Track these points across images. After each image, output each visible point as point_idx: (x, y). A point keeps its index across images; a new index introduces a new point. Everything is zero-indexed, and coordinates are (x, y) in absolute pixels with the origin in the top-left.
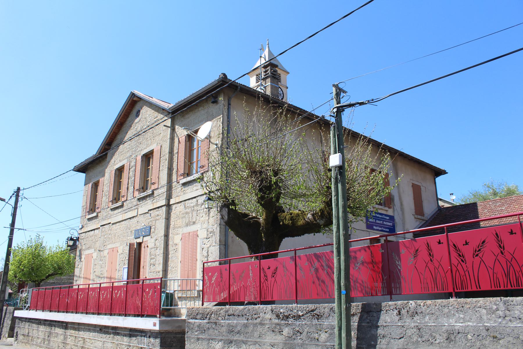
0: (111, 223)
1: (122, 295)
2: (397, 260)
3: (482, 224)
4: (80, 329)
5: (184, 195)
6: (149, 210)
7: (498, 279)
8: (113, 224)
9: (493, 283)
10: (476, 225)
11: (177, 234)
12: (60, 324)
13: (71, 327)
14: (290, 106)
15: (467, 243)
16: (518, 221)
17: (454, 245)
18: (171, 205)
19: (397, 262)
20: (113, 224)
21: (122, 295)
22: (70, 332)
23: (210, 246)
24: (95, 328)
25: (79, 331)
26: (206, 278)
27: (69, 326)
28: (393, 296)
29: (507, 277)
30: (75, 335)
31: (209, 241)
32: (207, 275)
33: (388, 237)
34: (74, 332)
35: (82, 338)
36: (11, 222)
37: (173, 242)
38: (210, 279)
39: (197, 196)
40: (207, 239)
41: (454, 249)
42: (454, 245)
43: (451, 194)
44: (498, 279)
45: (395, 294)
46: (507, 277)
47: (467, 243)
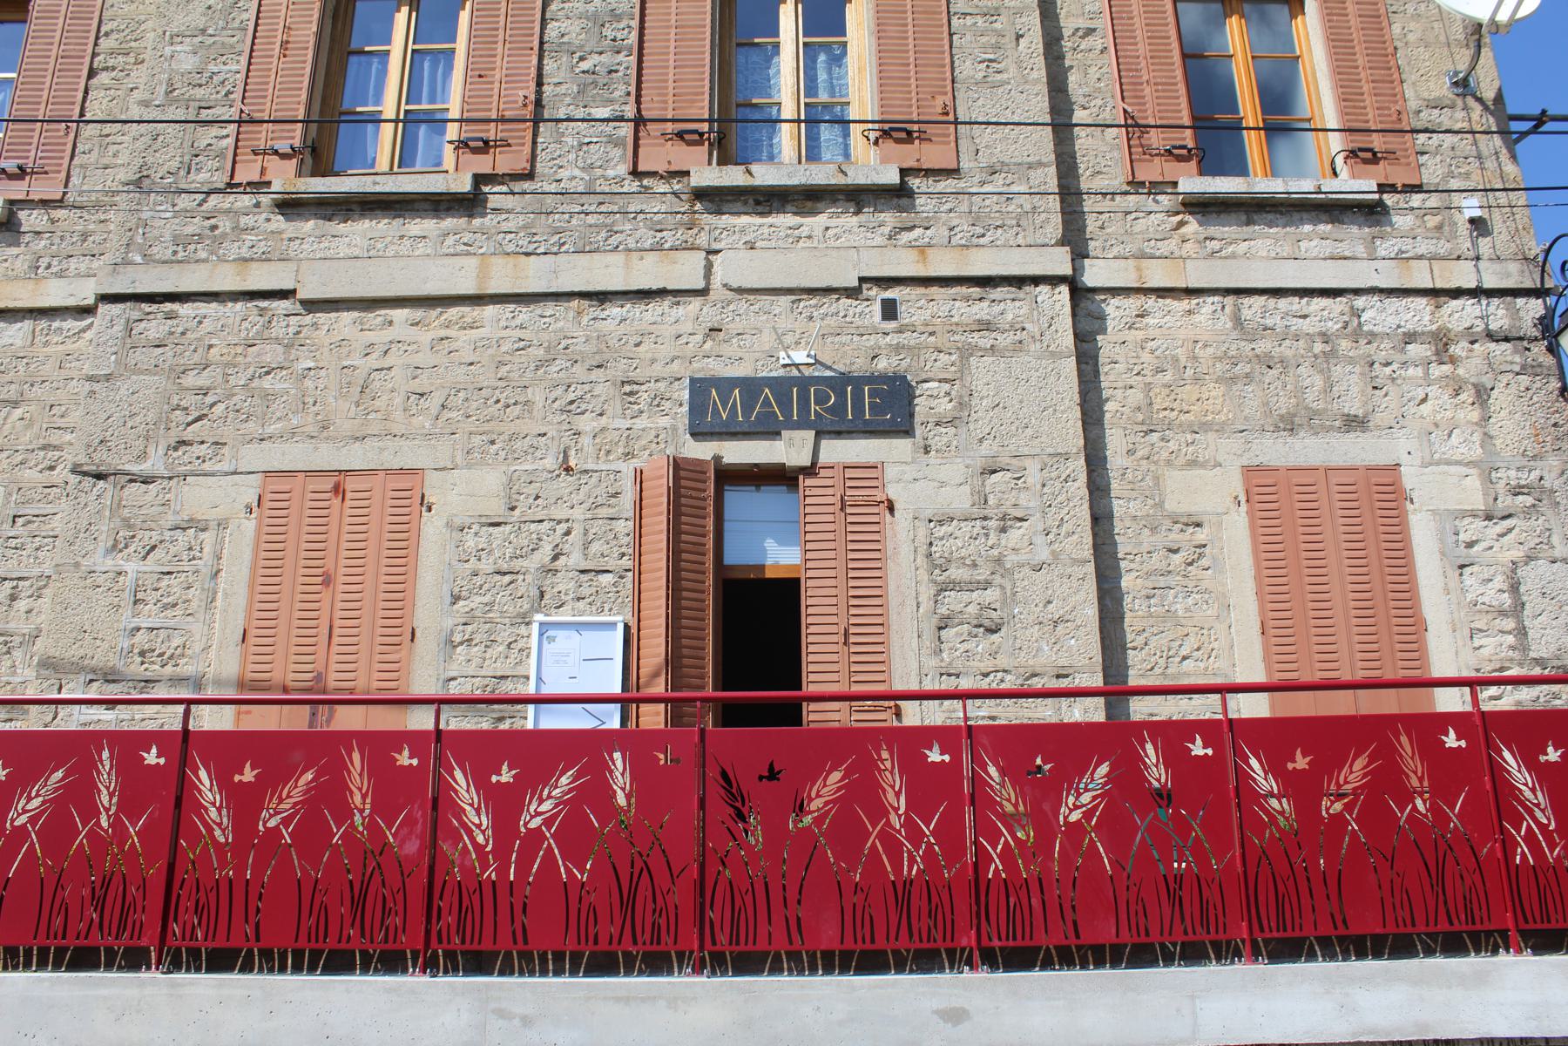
2: (893, 787)
3: (814, 714)
5: (1209, 262)
6: (862, 280)
7: (595, 913)
8: (312, 305)
9: (846, 917)
10: (790, 714)
11: (1193, 463)
15: (773, 775)
17: (724, 775)
18: (1094, 290)
19: (891, 795)
20: (312, 305)
23: (1529, 559)
29: (1173, 905)
31: (1510, 530)
33: (192, 706)
37: (1161, 505)
39: (1357, 292)
40: (1489, 518)
41: (722, 791)
42: (724, 775)
44: (595, 913)
46: (1173, 905)
47: (773, 775)
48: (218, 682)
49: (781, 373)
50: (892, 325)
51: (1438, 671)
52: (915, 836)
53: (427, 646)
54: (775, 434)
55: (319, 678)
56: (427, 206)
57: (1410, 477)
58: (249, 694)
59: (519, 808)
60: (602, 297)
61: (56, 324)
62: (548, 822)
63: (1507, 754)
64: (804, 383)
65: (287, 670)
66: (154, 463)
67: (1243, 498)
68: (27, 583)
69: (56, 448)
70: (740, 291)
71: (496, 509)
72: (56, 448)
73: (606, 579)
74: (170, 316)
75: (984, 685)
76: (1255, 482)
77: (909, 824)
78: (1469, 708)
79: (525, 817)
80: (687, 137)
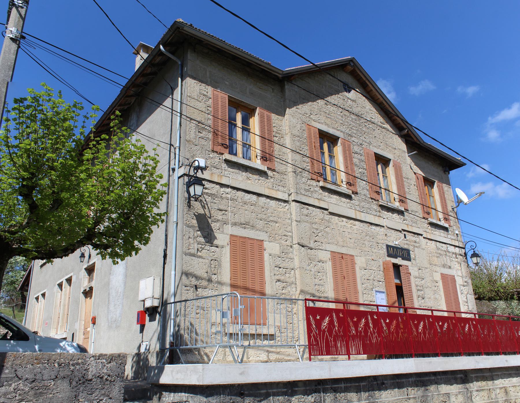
0: (423, 236)
1: (473, 329)
4: (494, 377)
6: (402, 229)
8: (331, 214)
12: (449, 376)
13: (476, 377)
14: (164, 42)
16: (210, 122)
20: (331, 214)
21: (473, 329)
22: (474, 386)
24: (517, 371)
25: (493, 379)
26: (313, 322)
27: (473, 375)
28: (351, 356)
30: (488, 388)
32: (315, 318)
34: (484, 383)
35: (501, 388)
36: (165, 265)
38: (318, 324)
43: (60, 92)
45: (352, 355)
48: (331, 299)
49: (394, 245)
50: (405, 239)
51: (462, 311)
52: (374, 333)
53: (360, 294)
54: (396, 258)
55: (347, 299)
56: (343, 195)
57: (266, 244)
58: (336, 302)
59: (321, 325)
60: (371, 224)
61: (280, 203)
62: (326, 328)
63: (334, 314)
64: (397, 248)
65: (342, 298)
66: (312, 245)
67: (229, 244)
68: (288, 270)
69: (287, 236)
70: (388, 228)
71: (365, 266)
72: (287, 236)
73: (381, 283)
74: (308, 209)
75: (424, 308)
76: (232, 239)
77: (373, 330)
78: (454, 316)
79: (322, 326)
80: (224, 145)
